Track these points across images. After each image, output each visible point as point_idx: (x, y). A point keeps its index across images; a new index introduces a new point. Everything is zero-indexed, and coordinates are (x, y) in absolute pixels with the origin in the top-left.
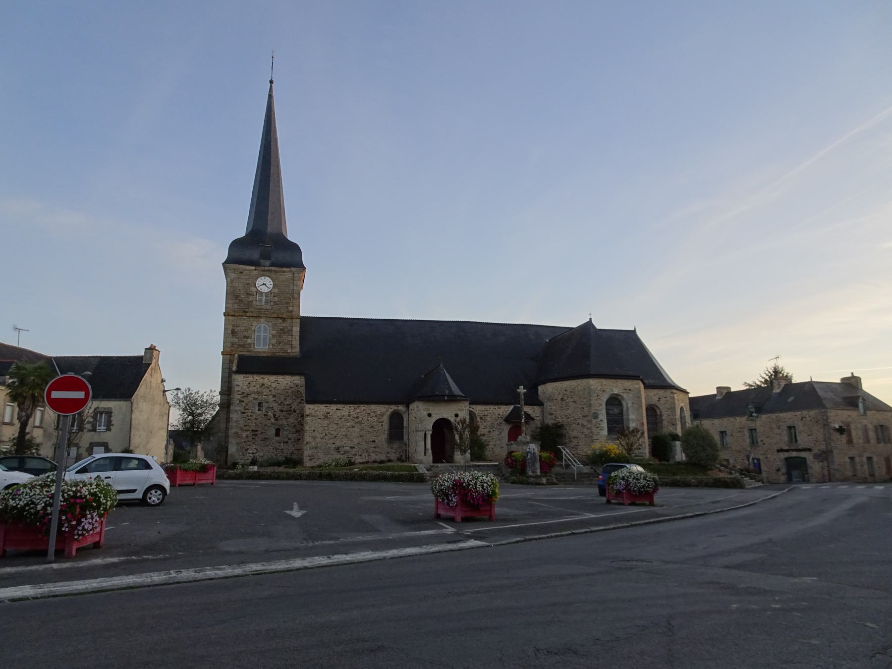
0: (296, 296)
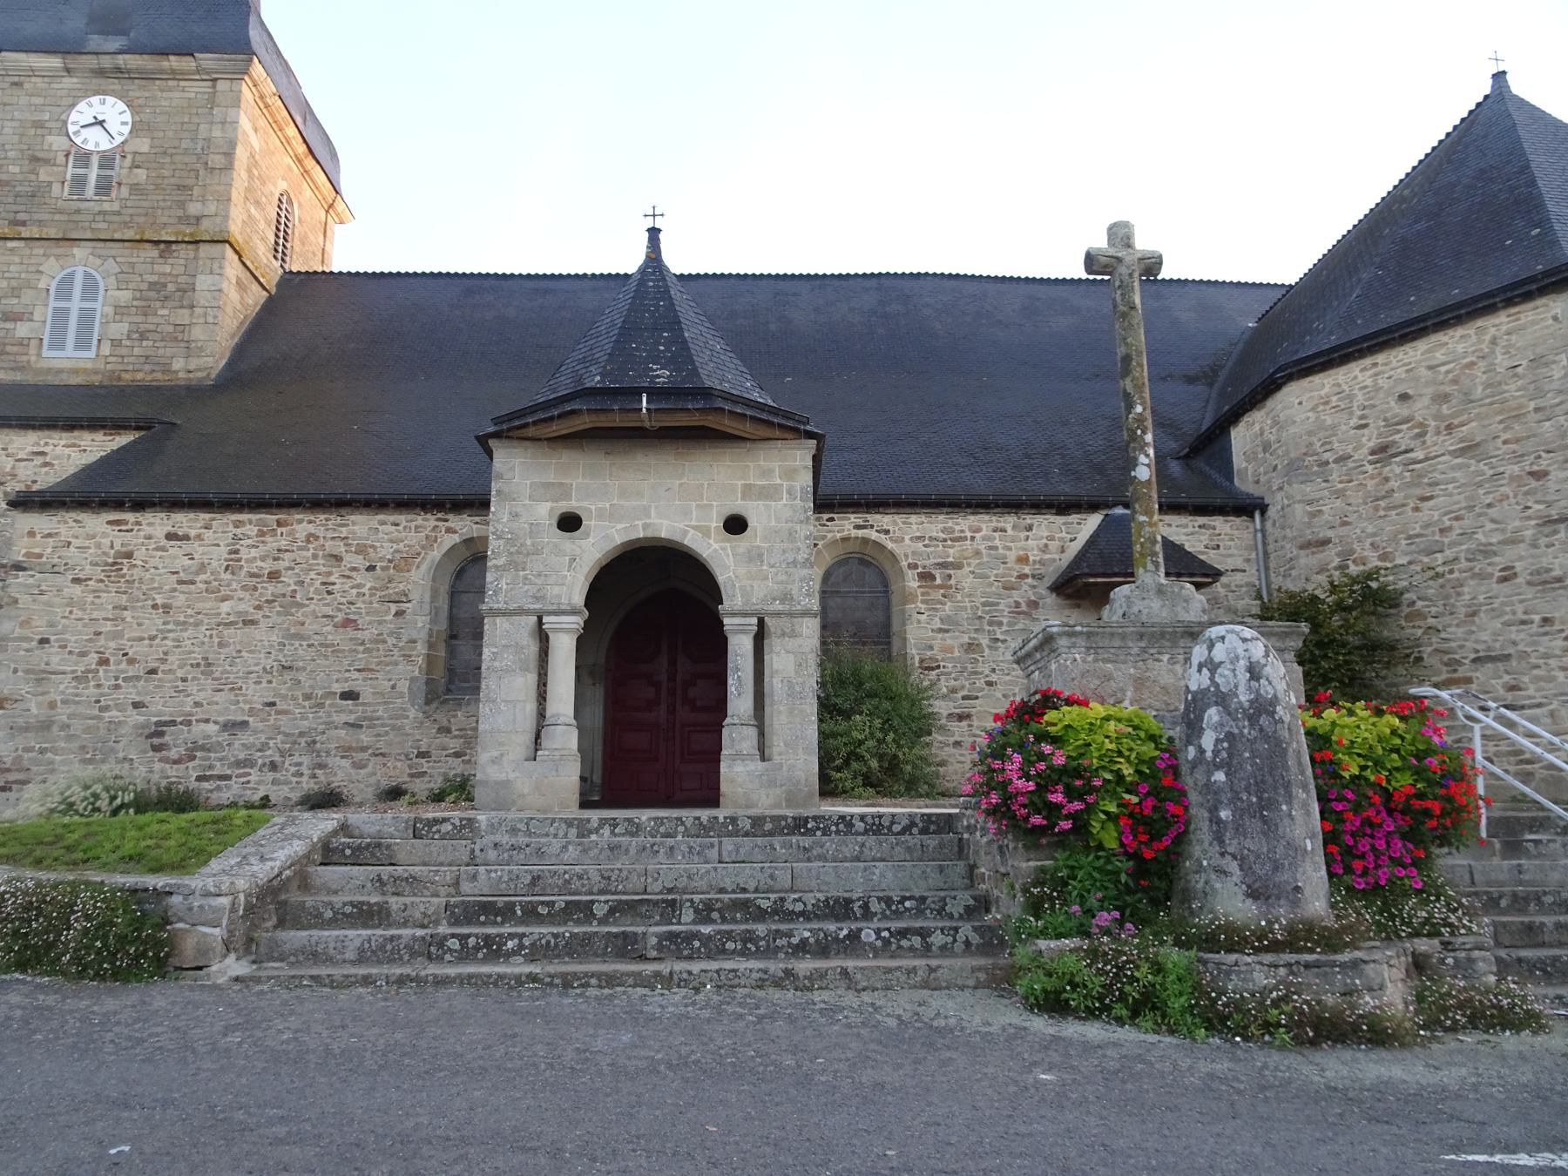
0: (216, 160)
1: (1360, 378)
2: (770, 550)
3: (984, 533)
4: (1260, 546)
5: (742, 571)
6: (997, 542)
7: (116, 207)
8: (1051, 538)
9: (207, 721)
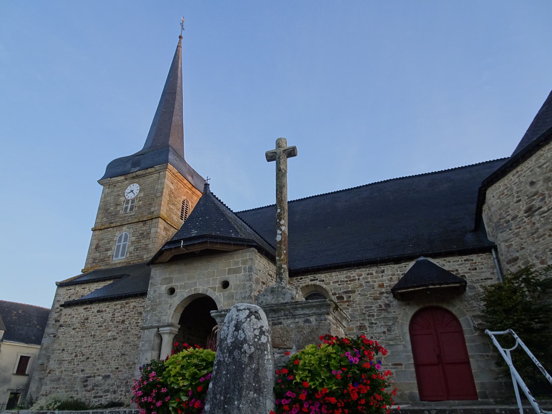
1: (513, 180)
2: (236, 293)
3: (363, 276)
4: (497, 266)
5: (226, 303)
6: (369, 280)
7: (134, 213)
8: (393, 275)
9: (99, 375)
